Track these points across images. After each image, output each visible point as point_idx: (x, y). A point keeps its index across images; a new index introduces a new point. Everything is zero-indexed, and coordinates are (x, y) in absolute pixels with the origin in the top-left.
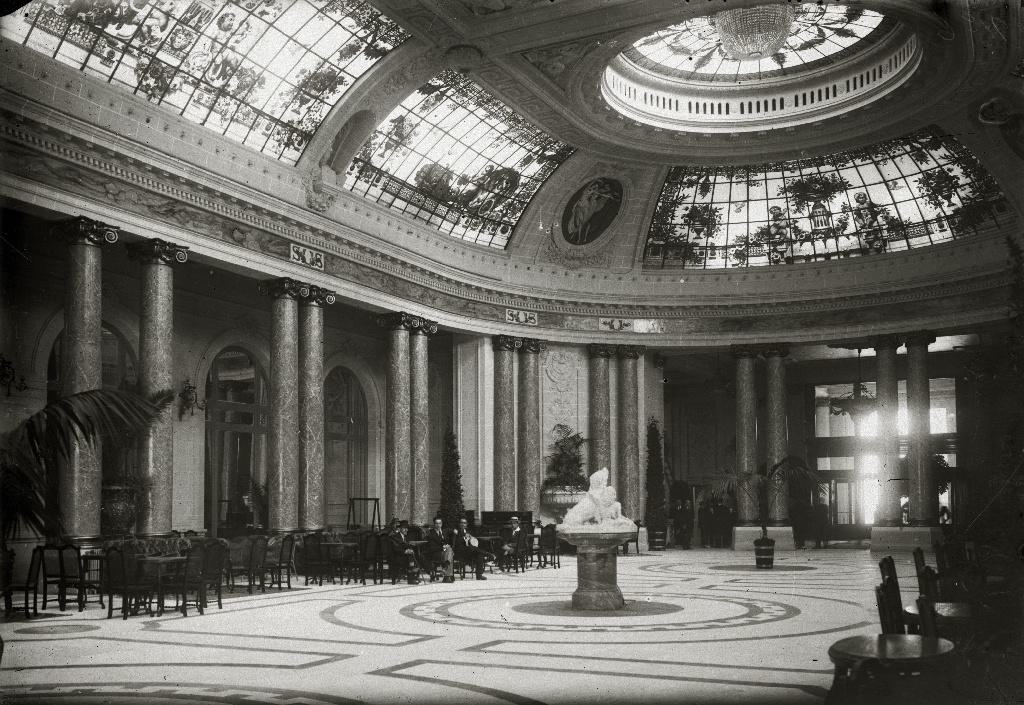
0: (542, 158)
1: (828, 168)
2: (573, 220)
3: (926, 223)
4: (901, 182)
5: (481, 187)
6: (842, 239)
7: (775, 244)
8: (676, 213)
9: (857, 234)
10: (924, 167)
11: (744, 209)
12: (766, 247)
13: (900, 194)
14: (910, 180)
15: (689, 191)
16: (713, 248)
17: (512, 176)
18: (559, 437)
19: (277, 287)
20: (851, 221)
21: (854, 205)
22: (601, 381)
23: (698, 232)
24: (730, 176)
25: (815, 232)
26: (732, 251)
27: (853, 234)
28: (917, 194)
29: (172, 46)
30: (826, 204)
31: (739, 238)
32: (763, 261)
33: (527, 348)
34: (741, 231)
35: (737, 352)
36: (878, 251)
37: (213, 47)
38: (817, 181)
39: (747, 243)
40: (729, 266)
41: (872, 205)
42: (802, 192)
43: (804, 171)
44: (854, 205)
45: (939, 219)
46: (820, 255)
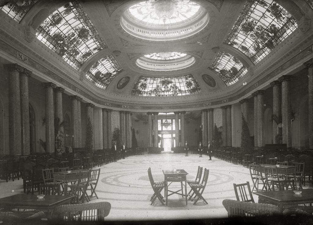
1: (170, 79)
3: (185, 91)
4: (182, 83)
6: (170, 92)
7: (157, 92)
8: (139, 84)
10: (187, 81)
12: (155, 93)
13: (182, 85)
15: (143, 80)
16: (145, 92)
17: (111, 74)
20: (172, 89)
21: (173, 86)
22: (122, 118)
23: (142, 88)
24: (151, 78)
25: (165, 91)
26: (148, 93)
28: (185, 85)
34: (151, 89)
38: (167, 81)
39: (151, 91)
41: (176, 87)
42: (163, 83)
43: (165, 79)
44: (173, 86)
45: (188, 90)
46: (165, 95)
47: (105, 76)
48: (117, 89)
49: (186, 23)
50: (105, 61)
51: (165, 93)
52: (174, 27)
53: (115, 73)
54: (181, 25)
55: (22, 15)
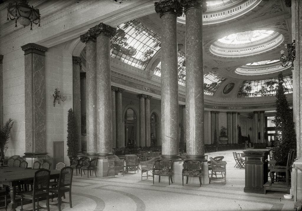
0: (221, 80)
5: (211, 86)
11: (257, 87)
12: (261, 93)
15: (247, 84)
16: (250, 94)
17: (216, 83)
18: (222, 128)
19: (140, 96)
23: (248, 91)
25: (270, 90)
26: (254, 94)
30: (273, 86)
31: (256, 92)
32: (260, 96)
35: (255, 112)
39: (257, 93)
40: (253, 97)
42: (268, 84)
46: (271, 95)
47: (211, 86)
48: (223, 94)
49: (269, 38)
50: (208, 75)
51: (271, 93)
52: (260, 42)
53: (220, 82)
54: (266, 40)
55: (145, 65)
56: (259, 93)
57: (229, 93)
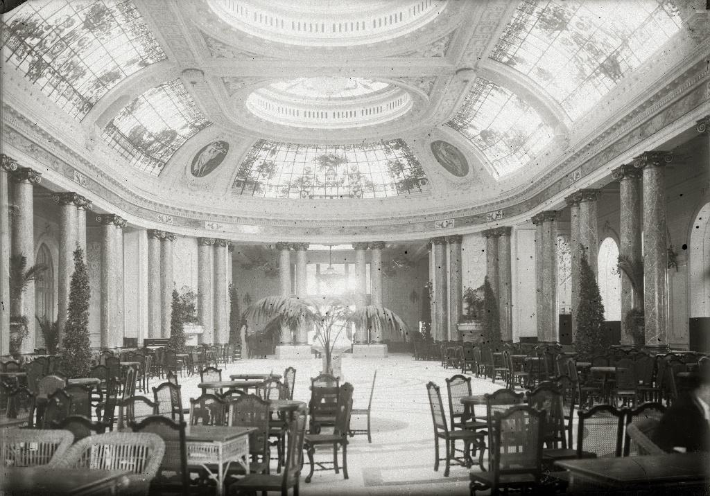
0: (193, 126)
2: (198, 162)
7: (305, 187)
9: (349, 186)
10: (389, 157)
14: (381, 163)
15: (262, 153)
23: (264, 176)
27: (347, 187)
29: (52, 52)
32: (296, 196)
33: (165, 238)
36: (359, 197)
37: (70, 54)
41: (358, 174)
42: (325, 160)
47: (157, 140)
56: (294, 186)
57: (209, 175)
